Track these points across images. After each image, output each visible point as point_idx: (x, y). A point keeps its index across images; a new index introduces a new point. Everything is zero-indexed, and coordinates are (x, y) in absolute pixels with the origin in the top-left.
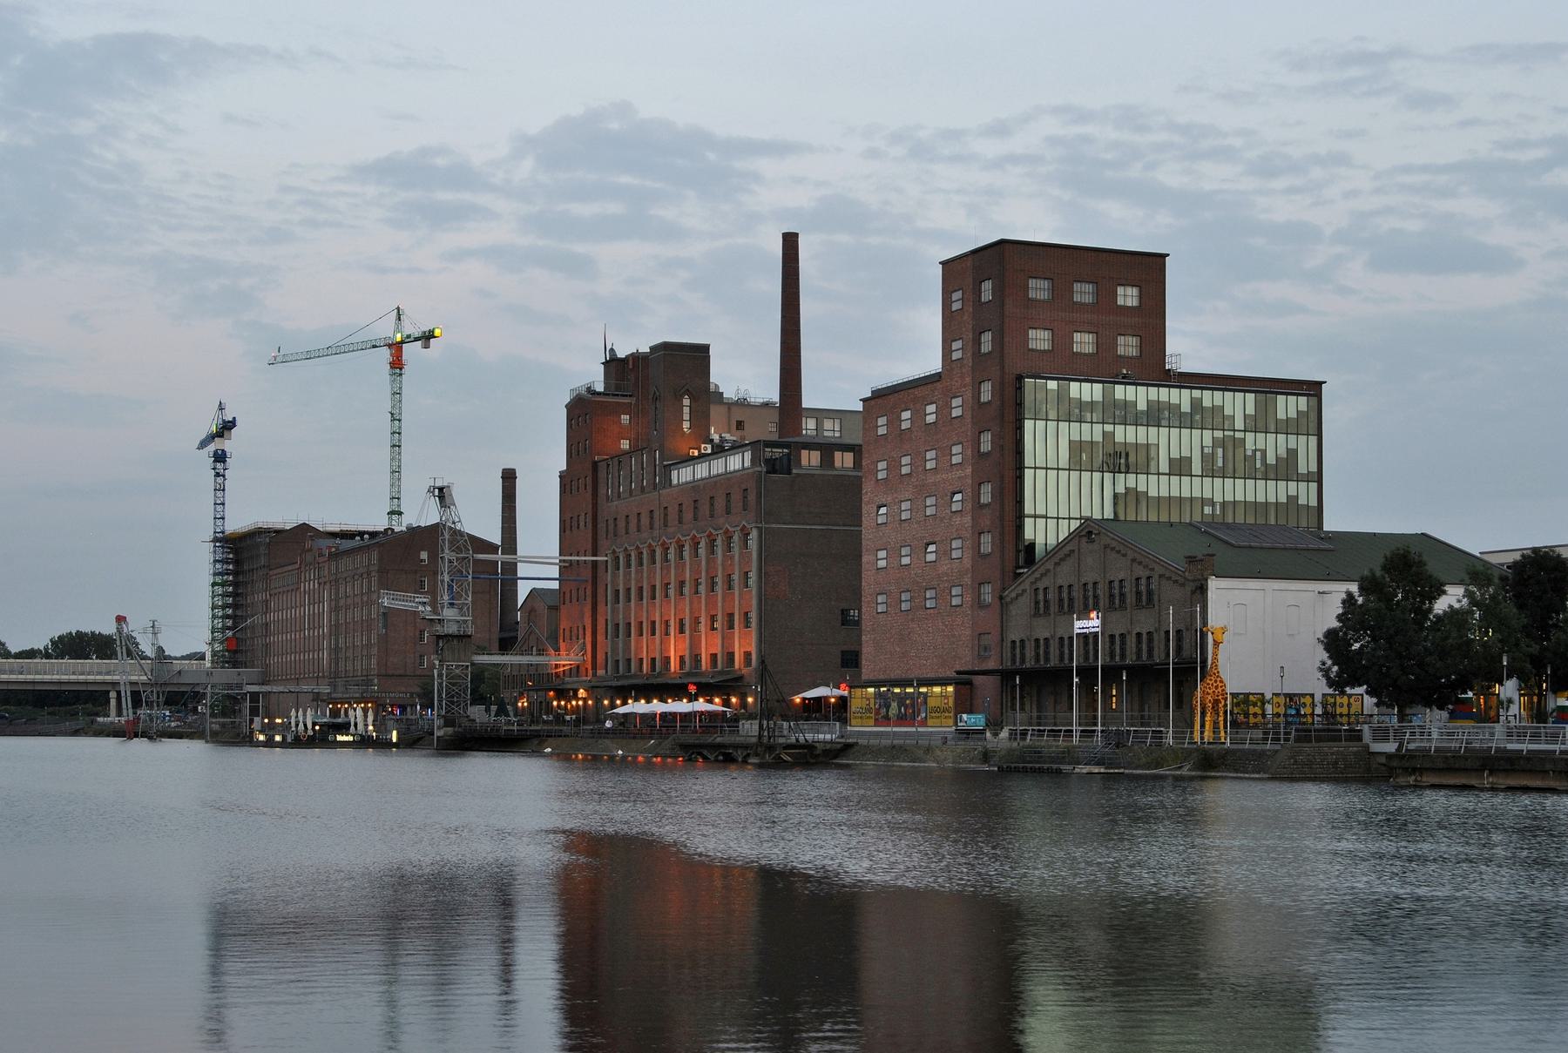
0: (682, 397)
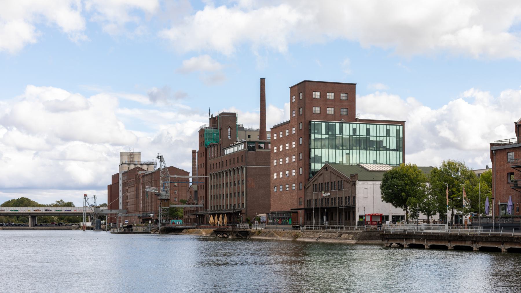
0: (228, 128)
